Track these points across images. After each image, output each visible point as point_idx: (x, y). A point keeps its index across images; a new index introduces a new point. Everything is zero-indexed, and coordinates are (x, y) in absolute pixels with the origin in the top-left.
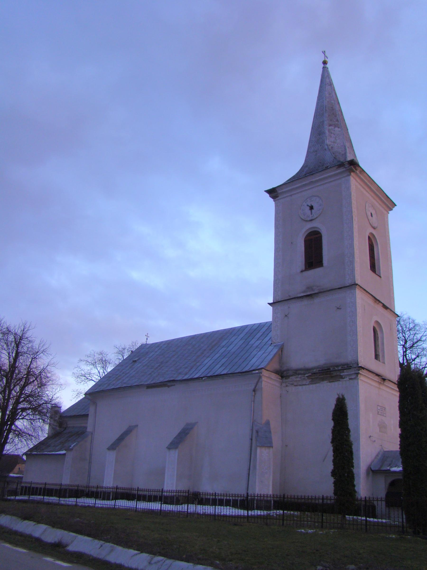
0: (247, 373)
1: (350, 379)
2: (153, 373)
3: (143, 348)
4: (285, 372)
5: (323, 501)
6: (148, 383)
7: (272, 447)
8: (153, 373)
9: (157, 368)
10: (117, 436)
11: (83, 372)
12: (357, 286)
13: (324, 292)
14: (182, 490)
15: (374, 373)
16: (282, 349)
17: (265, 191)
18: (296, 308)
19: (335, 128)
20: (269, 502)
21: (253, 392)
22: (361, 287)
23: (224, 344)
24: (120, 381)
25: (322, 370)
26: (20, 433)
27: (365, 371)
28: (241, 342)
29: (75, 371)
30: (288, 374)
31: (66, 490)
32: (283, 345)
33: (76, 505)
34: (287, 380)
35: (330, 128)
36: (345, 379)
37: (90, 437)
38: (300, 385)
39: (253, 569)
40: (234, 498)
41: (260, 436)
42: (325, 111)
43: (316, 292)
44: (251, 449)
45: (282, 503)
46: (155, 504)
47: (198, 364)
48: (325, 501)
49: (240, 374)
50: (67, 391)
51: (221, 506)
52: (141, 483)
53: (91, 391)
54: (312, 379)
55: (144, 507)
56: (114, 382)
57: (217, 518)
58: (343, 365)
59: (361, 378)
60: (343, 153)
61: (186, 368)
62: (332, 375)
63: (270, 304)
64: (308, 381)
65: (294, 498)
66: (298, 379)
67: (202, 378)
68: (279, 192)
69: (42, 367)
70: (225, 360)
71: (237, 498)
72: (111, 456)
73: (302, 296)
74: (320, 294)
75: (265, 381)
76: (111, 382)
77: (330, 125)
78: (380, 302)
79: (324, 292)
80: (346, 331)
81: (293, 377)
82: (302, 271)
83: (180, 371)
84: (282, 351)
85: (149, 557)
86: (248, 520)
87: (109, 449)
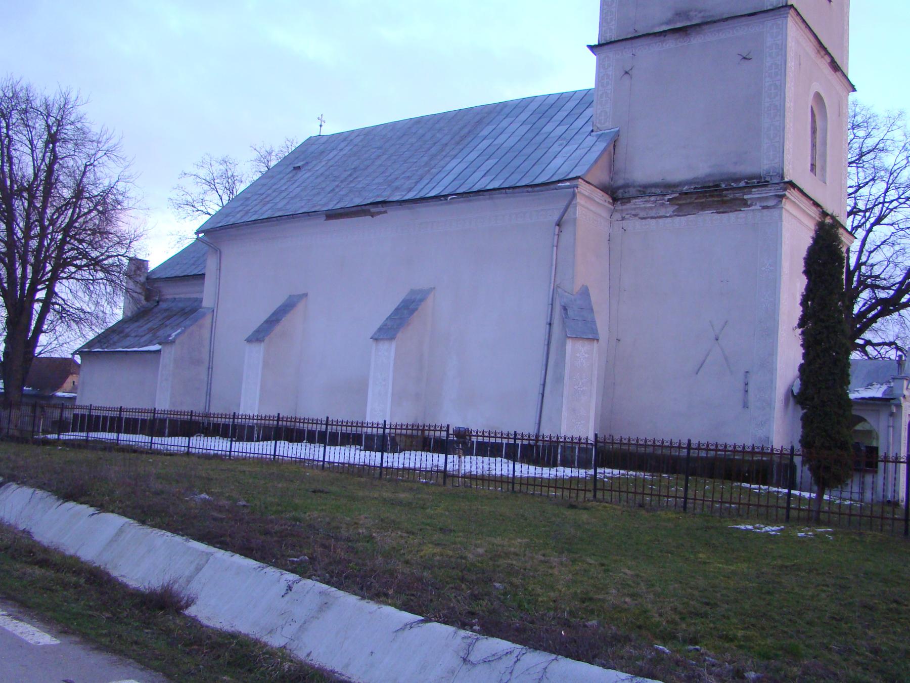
0: (547, 187)
1: (764, 208)
2: (337, 190)
3: (313, 144)
4: (621, 191)
5: (689, 453)
6: (330, 207)
7: (598, 340)
8: (337, 190)
9: (346, 178)
10: (264, 317)
11: (190, 199)
12: (792, 12)
13: (715, 22)
14: (405, 423)
15: (811, 199)
16: (614, 143)
20: (585, 451)
22: (798, 14)
23: (485, 132)
24: (269, 206)
26: (64, 309)
27: (795, 193)
28: (525, 128)
29: (173, 195)
30: (627, 195)
31: (163, 421)
32: (618, 134)
33: (188, 454)
34: (624, 207)
37: (207, 321)
38: (652, 218)
39: (794, 679)
40: (480, 439)
41: (571, 318)
43: (694, 22)
44: (549, 344)
45: (605, 452)
47: (434, 171)
48: (694, 454)
49: (530, 189)
50: (159, 234)
51: (483, 456)
52: (313, 408)
53: (208, 227)
54: (680, 205)
55: (341, 461)
56: (257, 208)
57: (517, 487)
59: (787, 205)
61: (409, 178)
62: (725, 198)
63: (591, 48)
64: (670, 210)
65: (629, 444)
67: (446, 196)
69: (106, 183)
70: (491, 162)
71: (499, 440)
72: (256, 354)
74: (704, 27)
75: (583, 206)
76: (249, 208)
78: (827, 53)
79: (715, 22)
80: (759, 106)
81: (638, 202)
83: (397, 183)
84: (614, 146)
85: (458, 640)
86: (595, 496)
87: (249, 340)
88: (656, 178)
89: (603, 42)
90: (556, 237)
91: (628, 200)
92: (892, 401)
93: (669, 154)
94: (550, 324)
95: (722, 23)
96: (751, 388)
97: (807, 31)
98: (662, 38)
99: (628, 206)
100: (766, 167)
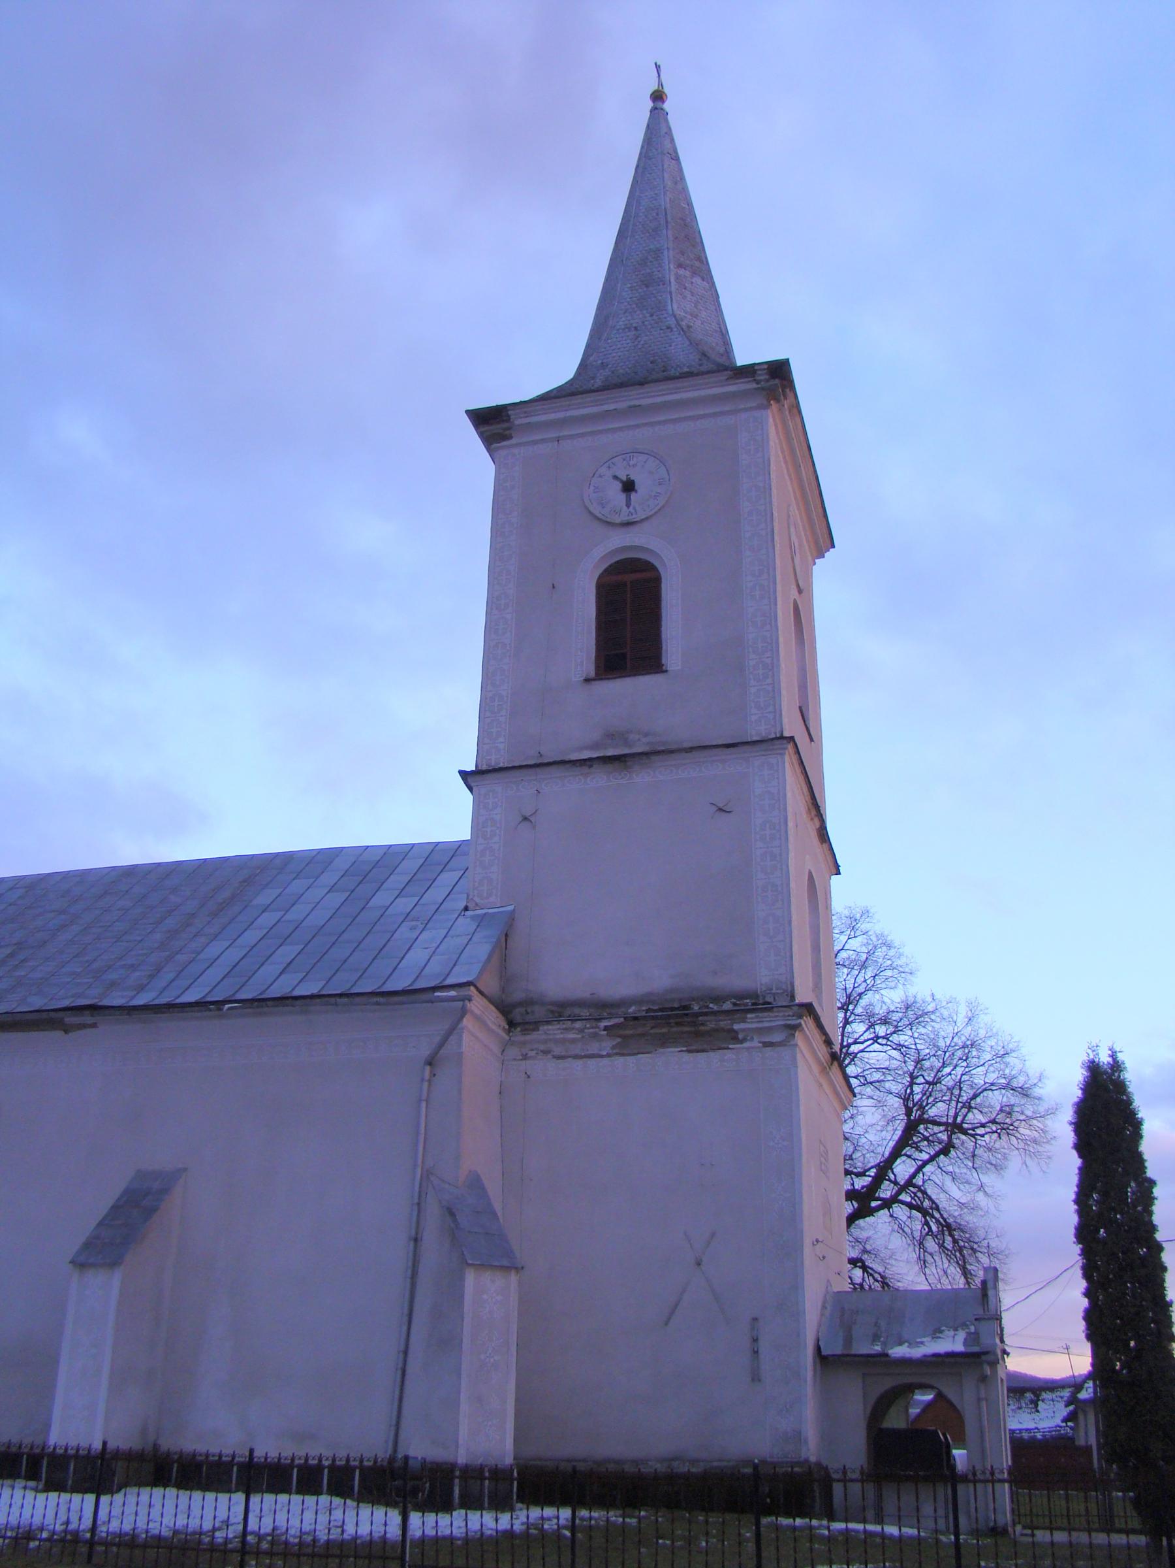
4: (518, 1010)
12: (790, 747)
13: (672, 752)
17: (468, 412)
18: (563, 795)
19: (692, 277)
21: (428, 1068)
25: (661, 1010)
28: (338, 898)
30: (529, 1018)
32: (511, 918)
34: (528, 1037)
35: (682, 272)
36: (746, 1045)
38: (576, 1057)
41: (463, 1231)
42: (663, 222)
45: (537, 1482)
46: (18, 1493)
47: (182, 958)
54: (624, 1037)
58: (740, 996)
60: (722, 350)
64: (607, 1045)
66: (571, 1036)
67: (219, 1004)
68: (517, 422)
73: (590, 759)
74: (654, 758)
77: (680, 266)
79: (672, 752)
81: (554, 1030)
82: (587, 680)
83: (113, 976)
88: (582, 993)
89: (484, 767)
90: (426, 1085)
91: (535, 1025)
92: (984, 1358)
93: (603, 952)
94: (416, 1240)
95: (684, 755)
96: (764, 1346)
97: (801, 778)
98: (585, 770)
99: (535, 1036)
100: (765, 980)
